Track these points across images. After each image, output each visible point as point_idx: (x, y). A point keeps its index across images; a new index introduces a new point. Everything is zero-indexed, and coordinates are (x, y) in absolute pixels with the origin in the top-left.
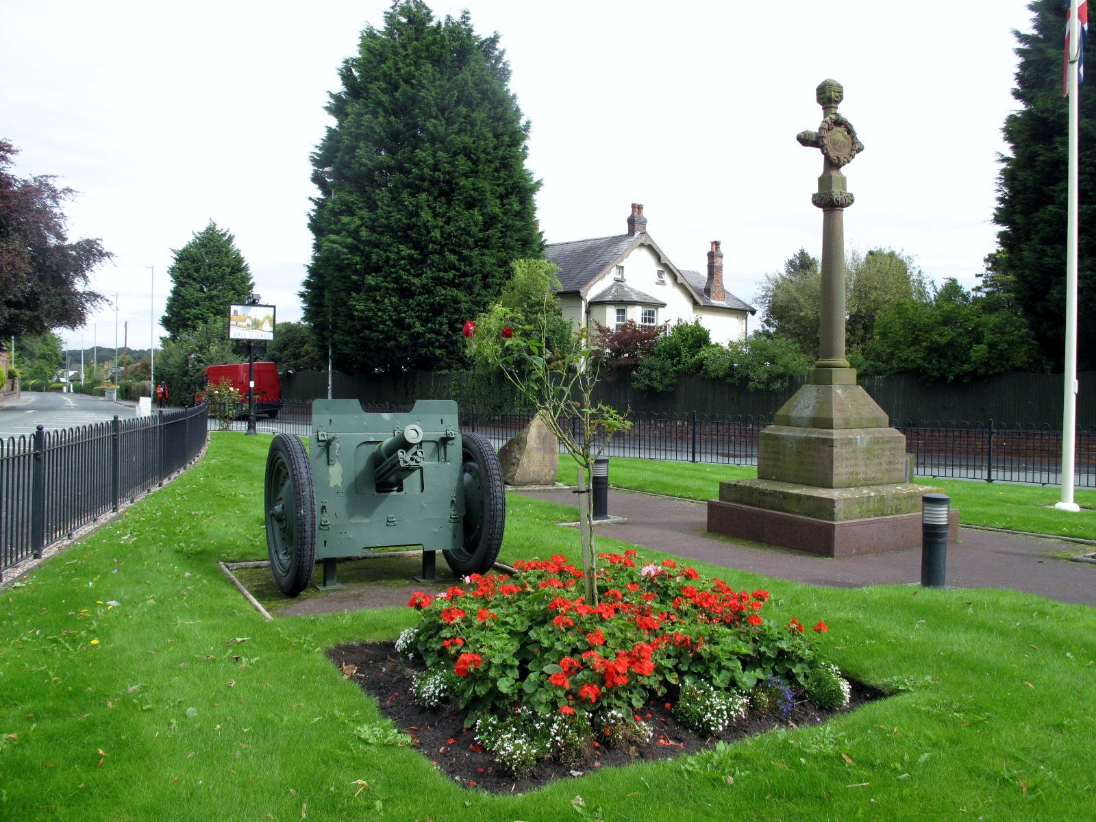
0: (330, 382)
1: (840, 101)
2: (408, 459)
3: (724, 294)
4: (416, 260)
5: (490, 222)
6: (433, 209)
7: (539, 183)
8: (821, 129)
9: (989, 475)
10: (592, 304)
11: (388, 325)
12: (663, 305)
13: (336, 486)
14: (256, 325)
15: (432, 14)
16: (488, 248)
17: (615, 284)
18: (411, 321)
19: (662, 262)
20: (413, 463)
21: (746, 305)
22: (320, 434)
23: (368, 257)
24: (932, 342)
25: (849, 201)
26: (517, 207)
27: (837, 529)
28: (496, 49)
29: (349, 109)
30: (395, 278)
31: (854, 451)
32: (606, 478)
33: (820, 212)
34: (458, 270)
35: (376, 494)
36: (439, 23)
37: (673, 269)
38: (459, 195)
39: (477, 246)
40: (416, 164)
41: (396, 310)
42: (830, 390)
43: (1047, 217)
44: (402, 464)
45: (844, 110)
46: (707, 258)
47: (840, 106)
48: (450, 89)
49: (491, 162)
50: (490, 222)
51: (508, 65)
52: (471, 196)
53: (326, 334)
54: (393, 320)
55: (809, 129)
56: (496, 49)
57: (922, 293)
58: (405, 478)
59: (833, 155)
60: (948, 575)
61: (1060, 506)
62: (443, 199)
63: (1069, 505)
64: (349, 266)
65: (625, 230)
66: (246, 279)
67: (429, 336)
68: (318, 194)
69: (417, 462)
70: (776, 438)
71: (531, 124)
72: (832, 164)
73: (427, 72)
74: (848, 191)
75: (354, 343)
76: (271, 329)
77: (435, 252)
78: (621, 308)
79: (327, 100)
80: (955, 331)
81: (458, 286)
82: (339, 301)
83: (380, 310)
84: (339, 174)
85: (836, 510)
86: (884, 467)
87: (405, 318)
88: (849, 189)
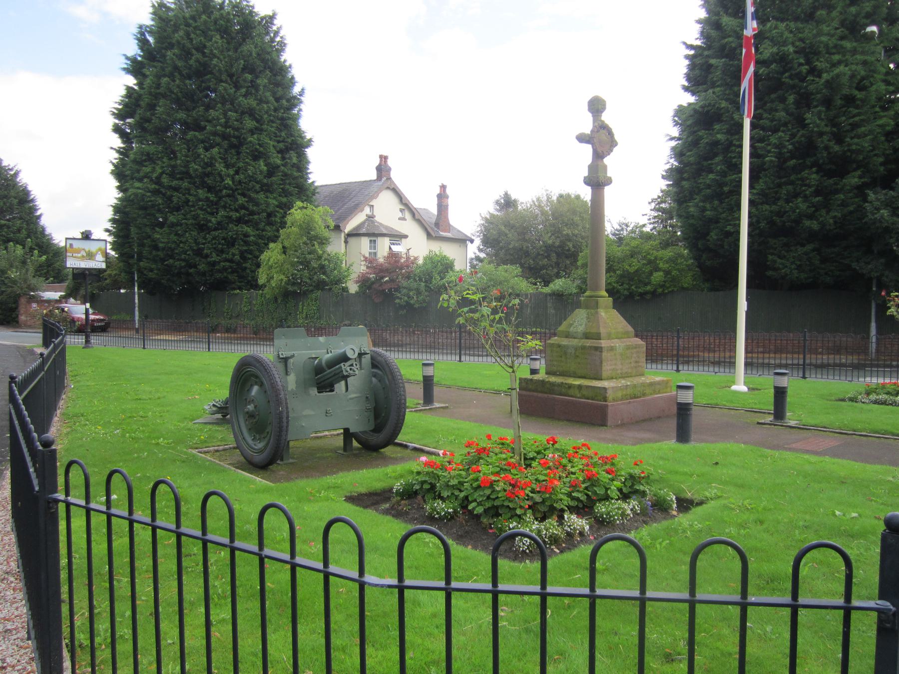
0: (137, 301)
2: (348, 369)
3: (449, 227)
4: (212, 201)
5: (272, 171)
6: (224, 159)
7: (310, 140)
8: (592, 131)
9: (678, 367)
10: (350, 235)
11: (189, 255)
12: (406, 237)
13: (292, 389)
14: (90, 256)
16: (271, 193)
17: (366, 220)
18: (209, 251)
20: (351, 372)
21: (466, 236)
22: (280, 353)
23: (170, 198)
24: (624, 271)
25: (609, 181)
26: (295, 160)
27: (610, 408)
28: (274, 25)
29: (146, 71)
30: (194, 215)
31: (615, 354)
32: (432, 376)
34: (246, 209)
35: (318, 394)
38: (247, 148)
39: (262, 190)
41: (197, 243)
42: (597, 313)
43: (708, 182)
44: (345, 374)
45: (606, 117)
46: (436, 199)
48: (237, 59)
49: (273, 122)
50: (272, 171)
51: (285, 39)
52: (256, 150)
53: (131, 261)
54: (193, 250)
56: (274, 25)
59: (599, 150)
60: (693, 436)
61: (734, 388)
62: (233, 151)
63: (741, 387)
64: (153, 206)
65: (373, 176)
66: (34, 209)
68: (118, 142)
69: (354, 371)
70: (559, 346)
72: (599, 156)
73: (217, 43)
74: (609, 175)
75: (159, 270)
76: (104, 259)
77: (228, 196)
79: (124, 63)
82: (144, 234)
83: (181, 242)
84: (141, 126)
85: (608, 395)
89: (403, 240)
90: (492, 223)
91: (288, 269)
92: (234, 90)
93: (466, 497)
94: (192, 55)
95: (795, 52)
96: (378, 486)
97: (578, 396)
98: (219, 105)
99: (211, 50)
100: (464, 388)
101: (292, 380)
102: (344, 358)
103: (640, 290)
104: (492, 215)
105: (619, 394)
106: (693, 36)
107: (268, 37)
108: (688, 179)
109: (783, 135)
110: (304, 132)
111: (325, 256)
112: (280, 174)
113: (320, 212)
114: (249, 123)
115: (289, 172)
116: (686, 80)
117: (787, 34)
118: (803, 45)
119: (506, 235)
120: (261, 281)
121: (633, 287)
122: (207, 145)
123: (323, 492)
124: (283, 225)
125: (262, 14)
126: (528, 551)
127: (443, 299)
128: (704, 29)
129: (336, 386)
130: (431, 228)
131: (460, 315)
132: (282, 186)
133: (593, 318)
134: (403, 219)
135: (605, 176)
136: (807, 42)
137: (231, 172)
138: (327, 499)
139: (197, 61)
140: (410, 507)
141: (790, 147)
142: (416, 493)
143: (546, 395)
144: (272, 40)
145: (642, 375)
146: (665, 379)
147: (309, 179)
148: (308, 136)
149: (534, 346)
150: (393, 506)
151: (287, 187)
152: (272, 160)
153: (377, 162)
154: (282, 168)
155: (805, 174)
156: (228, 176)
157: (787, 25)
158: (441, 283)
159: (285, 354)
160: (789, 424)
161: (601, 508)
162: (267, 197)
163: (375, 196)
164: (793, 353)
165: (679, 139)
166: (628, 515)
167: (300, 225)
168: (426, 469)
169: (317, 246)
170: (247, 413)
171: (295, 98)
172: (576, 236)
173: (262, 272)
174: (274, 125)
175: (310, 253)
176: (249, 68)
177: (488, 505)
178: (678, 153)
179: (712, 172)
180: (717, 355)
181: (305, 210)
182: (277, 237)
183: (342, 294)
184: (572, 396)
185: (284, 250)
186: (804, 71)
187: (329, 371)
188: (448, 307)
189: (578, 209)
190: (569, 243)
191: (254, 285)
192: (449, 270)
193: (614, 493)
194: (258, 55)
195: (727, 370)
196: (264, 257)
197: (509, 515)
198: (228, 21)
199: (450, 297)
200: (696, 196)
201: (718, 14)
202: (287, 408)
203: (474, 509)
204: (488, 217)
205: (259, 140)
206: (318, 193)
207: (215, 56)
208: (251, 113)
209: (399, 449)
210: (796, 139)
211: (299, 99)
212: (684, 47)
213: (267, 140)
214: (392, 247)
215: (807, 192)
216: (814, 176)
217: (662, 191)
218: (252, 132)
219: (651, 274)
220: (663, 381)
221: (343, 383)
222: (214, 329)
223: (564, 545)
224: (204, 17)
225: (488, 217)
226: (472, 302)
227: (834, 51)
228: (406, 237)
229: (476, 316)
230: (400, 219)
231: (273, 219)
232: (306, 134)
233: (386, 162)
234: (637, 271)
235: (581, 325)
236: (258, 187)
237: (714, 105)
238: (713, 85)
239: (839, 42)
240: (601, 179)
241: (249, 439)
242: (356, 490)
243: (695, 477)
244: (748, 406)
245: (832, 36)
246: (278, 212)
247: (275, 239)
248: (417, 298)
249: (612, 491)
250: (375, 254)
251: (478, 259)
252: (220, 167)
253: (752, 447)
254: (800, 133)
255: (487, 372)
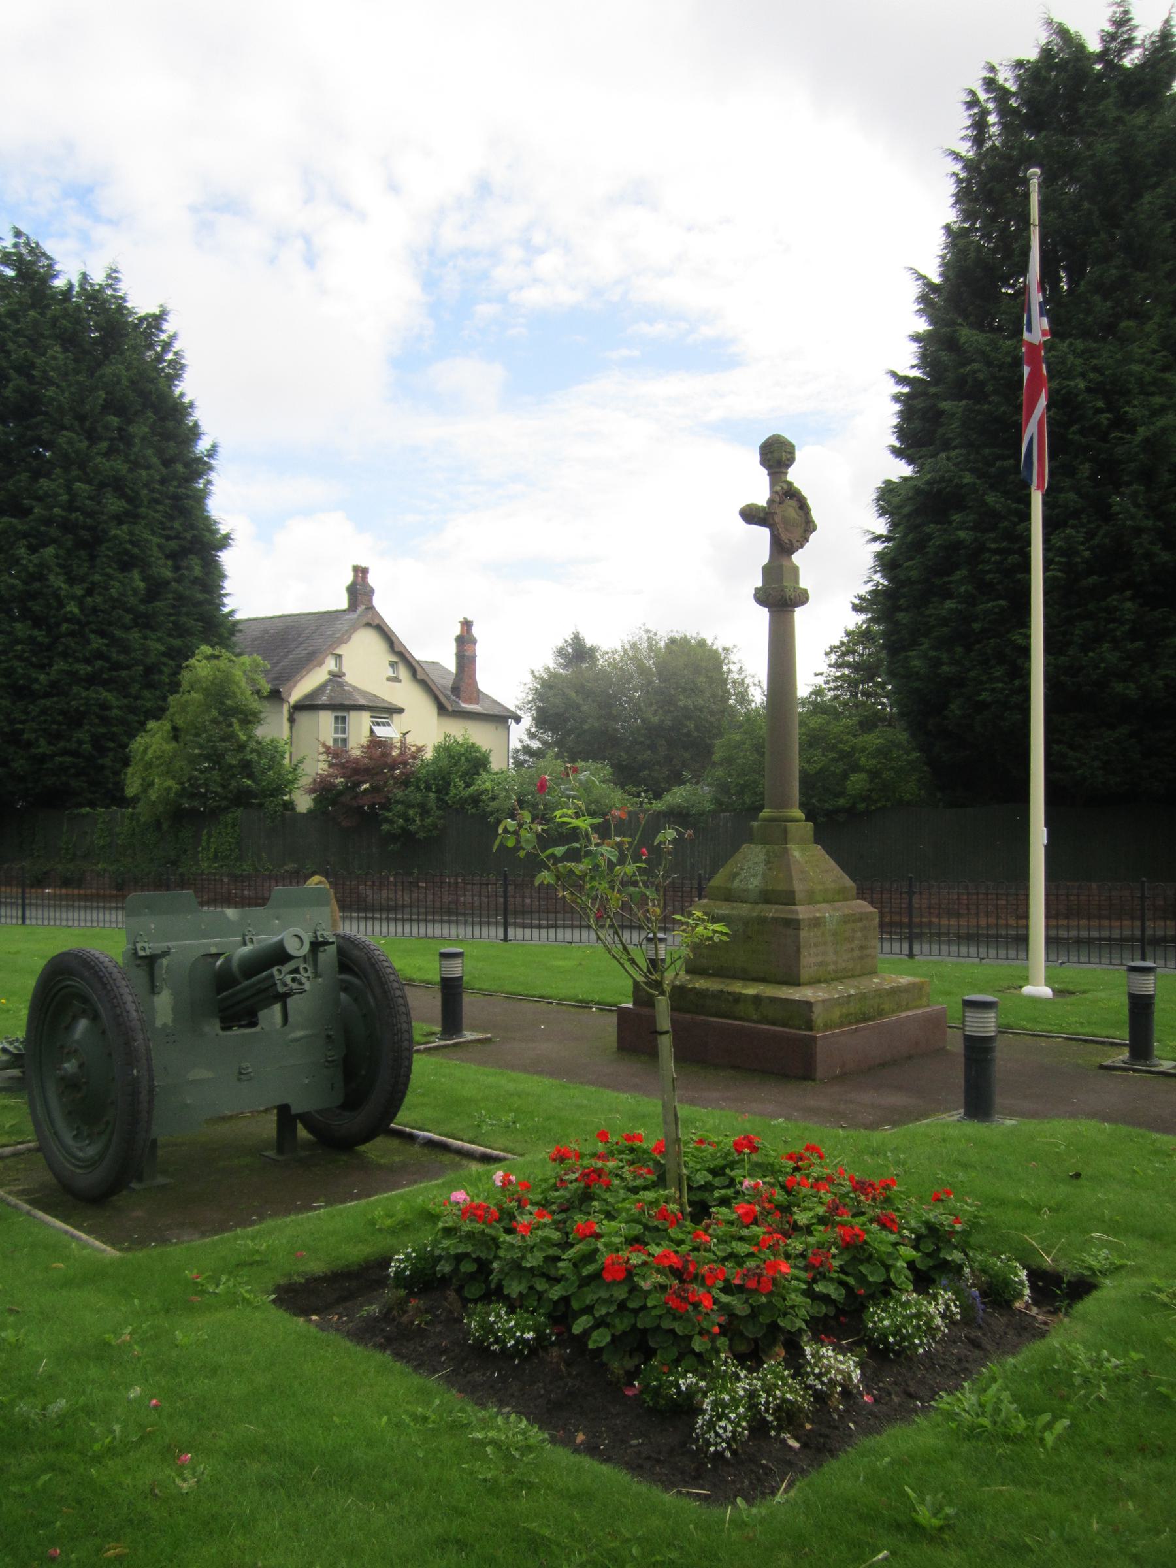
1: (792, 464)
2: (288, 979)
3: (476, 695)
5: (155, 590)
7: (227, 537)
10: (300, 707)
12: (400, 711)
13: (165, 1025)
15: (57, 267)
16: (154, 630)
17: (329, 680)
19: (396, 649)
20: (295, 986)
21: (507, 709)
22: (139, 946)
25: (802, 598)
27: (819, 1043)
28: (163, 331)
31: (823, 934)
33: (763, 614)
34: (106, 658)
35: (221, 1032)
36: (71, 286)
37: (411, 659)
38: (108, 549)
39: (137, 625)
40: (39, 499)
42: (786, 851)
44: (281, 989)
47: (790, 470)
49: (157, 502)
50: (155, 590)
51: (183, 357)
52: (127, 552)
55: (755, 502)
56: (163, 331)
57: (743, 698)
58: (262, 1009)
59: (785, 537)
60: (999, 1100)
61: (1028, 990)
62: (83, 553)
65: (342, 603)
67: (60, 759)
69: (301, 984)
71: (219, 449)
72: (782, 548)
73: (55, 358)
77: (72, 634)
78: (340, 714)
80: (826, 756)
81: (105, 683)
85: (814, 1017)
86: (857, 953)
87: (23, 730)
88: (803, 584)
89: (396, 717)
90: (551, 687)
91: (182, 769)
92: (85, 443)
93: (565, 1300)
94: (9, 380)
95: (1089, 390)
96: (355, 1253)
97: (755, 1017)
98: (58, 470)
99: (45, 372)
100: (517, 997)
101: (164, 1001)
102: (279, 956)
103: (827, 806)
104: (553, 675)
105: (836, 1014)
106: (907, 359)
107: (151, 353)
108: (906, 610)
109: (1073, 532)
110: (215, 523)
111: (253, 744)
112: (170, 596)
113: (243, 664)
114: (114, 504)
115: (187, 593)
116: (898, 438)
117: (1071, 358)
118: (1100, 379)
119: (578, 707)
120: (131, 791)
121: (814, 801)
122: (34, 541)
123: (224, 1278)
124: (175, 687)
125: (142, 312)
126: (728, 1454)
127: (506, 831)
128: (926, 350)
129: (262, 1014)
130: (446, 696)
131: (543, 866)
132: (172, 618)
133: (779, 860)
134: (395, 679)
135: (796, 588)
136: (1107, 373)
137: (79, 591)
138: (233, 1300)
139: (18, 390)
140: (429, 1317)
141: (1087, 554)
142: (445, 1281)
143: (688, 1017)
144: (159, 358)
145: (874, 972)
146: (917, 980)
147: (224, 605)
148: (223, 529)
149: (710, 934)
150: (390, 1310)
151: (183, 619)
152: (154, 571)
153: (349, 578)
154: (174, 585)
155: (1113, 600)
156: (73, 597)
157: (1071, 344)
158: (466, 793)
159: (147, 947)
160: (1161, 1069)
161: (880, 1319)
162: (145, 638)
163: (344, 639)
164: (1100, 917)
165: (888, 539)
166: (938, 1328)
167: (206, 689)
168: (467, 1227)
169: (237, 726)
170: (63, 1078)
171: (199, 460)
172: (701, 711)
173: (133, 775)
174: (160, 508)
175: (223, 739)
176: (114, 406)
177: (621, 1325)
178: (887, 563)
179: (950, 596)
180: (963, 923)
181: (215, 662)
182: (163, 710)
183: (283, 815)
184: (741, 1019)
185: (176, 734)
186: (1106, 422)
187: (246, 983)
188: (518, 847)
189: (704, 664)
190: (688, 723)
191: (117, 798)
192: (481, 771)
193: (901, 1276)
194: (133, 382)
195: (1012, 953)
196: (138, 743)
197: (674, 1353)
198: (78, 321)
199: (521, 825)
200: (923, 639)
201: (953, 323)
202: (150, 1069)
203: (586, 1333)
204: (546, 676)
205: (131, 533)
206: (240, 631)
207: (51, 382)
208: (117, 485)
209: (395, 1143)
210: (1096, 541)
211: (206, 463)
212: (892, 381)
213: (147, 535)
214: (376, 728)
215: (1118, 633)
216: (1129, 605)
217: (848, 634)
218: (119, 519)
219: (845, 776)
220: (914, 984)
221: (277, 1007)
222: (40, 882)
223: (808, 1426)
224: (32, 313)
225: (546, 676)
226: (575, 834)
227: (1153, 389)
228: (400, 711)
229: (580, 868)
230: (390, 679)
231: (156, 677)
232: (220, 526)
233: (364, 578)
234: (821, 771)
235: (755, 876)
236: (128, 618)
237: (950, 480)
238: (946, 446)
239: (1161, 375)
240: (789, 593)
241: (68, 1137)
242: (302, 1269)
243: (1046, 1215)
244: (1071, 1030)
245: (1149, 364)
246: (165, 664)
247: (158, 713)
248: (422, 820)
249: (898, 1272)
250: (344, 741)
251: (527, 750)
252: (57, 581)
253: (1124, 1129)
254: (1102, 532)
255: (561, 963)
